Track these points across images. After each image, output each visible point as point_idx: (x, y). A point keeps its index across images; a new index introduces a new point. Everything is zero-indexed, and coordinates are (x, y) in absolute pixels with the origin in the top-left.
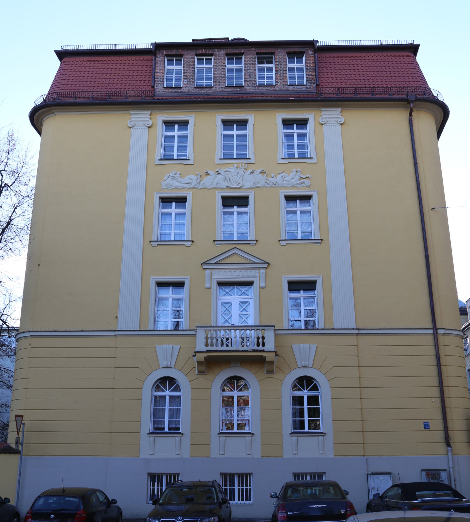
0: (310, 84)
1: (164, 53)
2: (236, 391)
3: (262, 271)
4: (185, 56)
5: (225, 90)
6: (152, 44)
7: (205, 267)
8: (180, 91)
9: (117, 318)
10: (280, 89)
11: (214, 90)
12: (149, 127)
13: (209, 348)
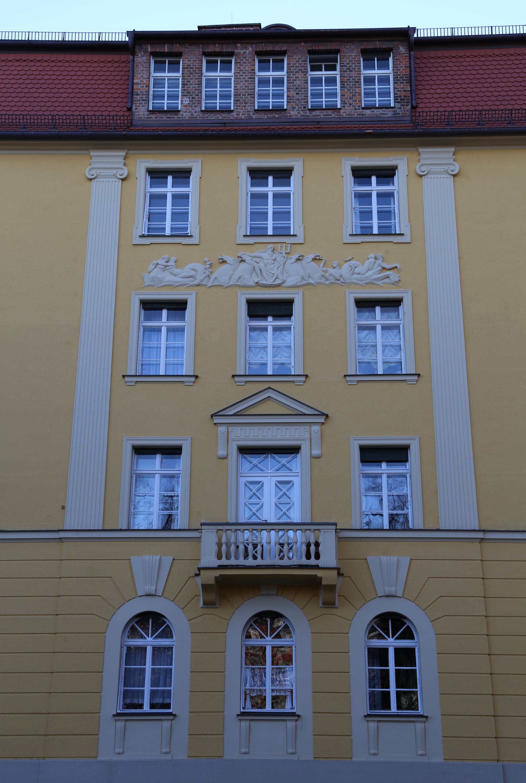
0: (401, 105)
1: (149, 50)
2: (269, 638)
3: (316, 428)
4: (185, 56)
5: (254, 117)
6: (128, 33)
7: (217, 420)
8: (176, 117)
9: (63, 508)
10: (349, 114)
11: (235, 116)
12: (123, 180)
13: (224, 561)
